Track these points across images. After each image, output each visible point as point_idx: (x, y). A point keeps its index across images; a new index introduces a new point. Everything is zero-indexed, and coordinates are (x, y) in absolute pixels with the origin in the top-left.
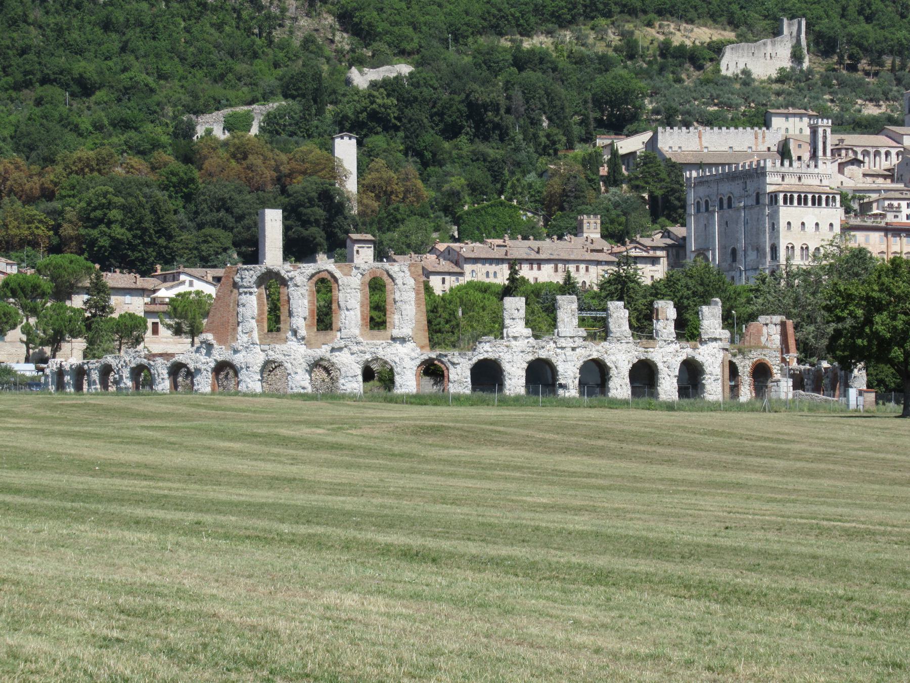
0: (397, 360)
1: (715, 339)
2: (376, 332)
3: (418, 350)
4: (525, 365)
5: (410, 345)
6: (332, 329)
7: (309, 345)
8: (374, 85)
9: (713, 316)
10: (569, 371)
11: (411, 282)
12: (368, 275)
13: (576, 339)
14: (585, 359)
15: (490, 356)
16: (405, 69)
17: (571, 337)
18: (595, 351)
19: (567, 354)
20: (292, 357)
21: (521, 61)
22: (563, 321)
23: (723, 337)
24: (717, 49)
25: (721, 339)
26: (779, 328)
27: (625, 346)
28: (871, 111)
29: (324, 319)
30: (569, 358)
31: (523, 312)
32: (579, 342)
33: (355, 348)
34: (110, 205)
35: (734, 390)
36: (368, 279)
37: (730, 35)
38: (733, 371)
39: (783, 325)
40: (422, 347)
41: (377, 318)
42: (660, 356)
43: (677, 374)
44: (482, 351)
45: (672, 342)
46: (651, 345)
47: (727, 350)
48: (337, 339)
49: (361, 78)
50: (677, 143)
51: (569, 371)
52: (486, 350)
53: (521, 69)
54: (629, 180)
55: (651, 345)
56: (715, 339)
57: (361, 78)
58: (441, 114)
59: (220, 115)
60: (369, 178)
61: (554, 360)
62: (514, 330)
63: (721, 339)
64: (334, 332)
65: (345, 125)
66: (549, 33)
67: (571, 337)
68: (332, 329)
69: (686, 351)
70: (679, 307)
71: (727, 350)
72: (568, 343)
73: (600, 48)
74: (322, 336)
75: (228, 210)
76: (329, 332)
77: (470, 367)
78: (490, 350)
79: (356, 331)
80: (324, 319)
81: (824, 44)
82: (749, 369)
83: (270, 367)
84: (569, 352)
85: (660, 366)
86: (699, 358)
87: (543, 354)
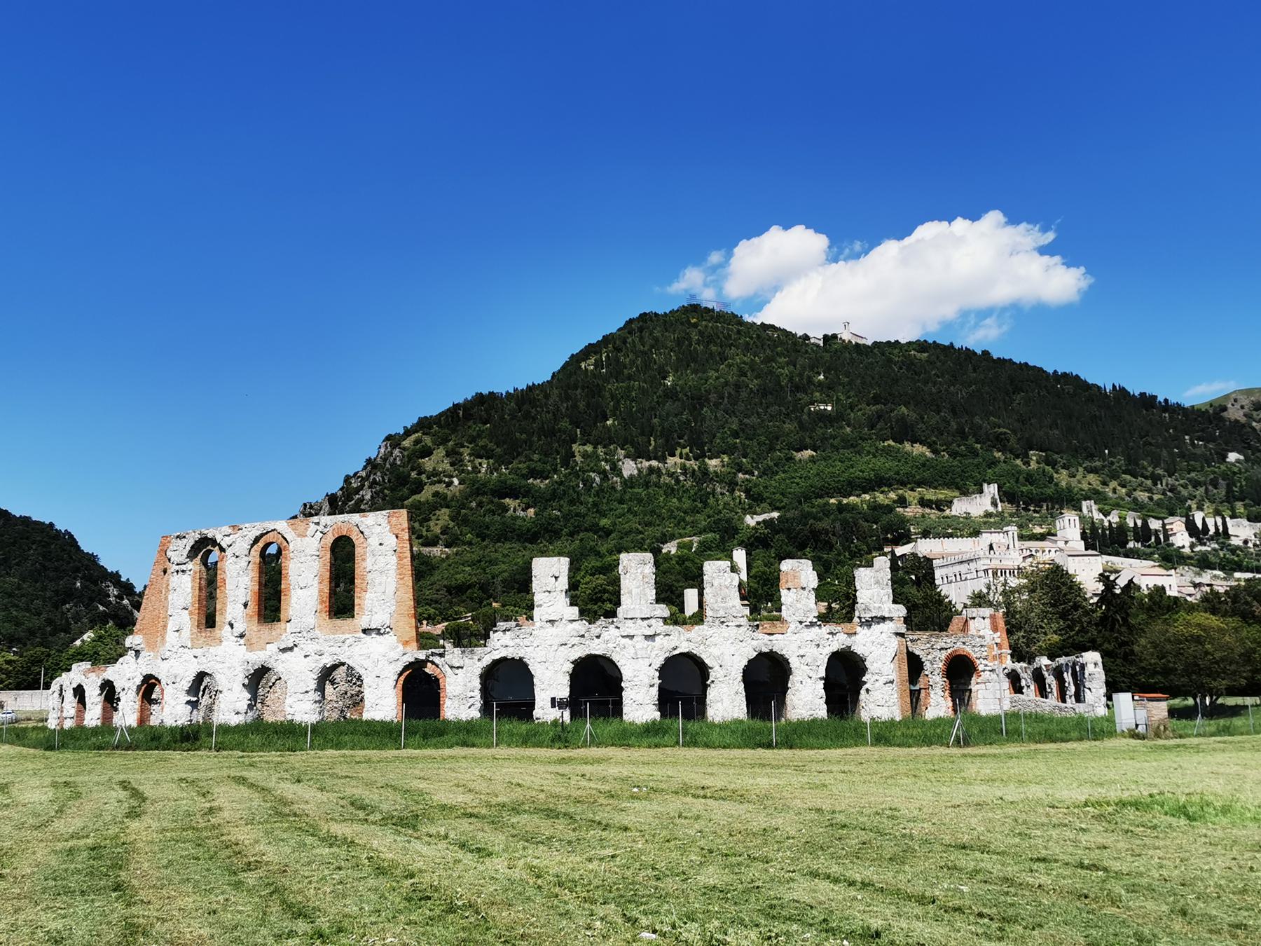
0: (367, 663)
1: (883, 619)
2: (339, 622)
3: (401, 647)
4: (569, 667)
5: (390, 639)
6: (279, 620)
7: (250, 646)
8: (758, 523)
9: (877, 582)
10: (551, 684)
11: (391, 541)
12: (330, 534)
13: (653, 621)
14: (667, 655)
15: (509, 653)
16: (775, 515)
17: (643, 619)
18: (682, 640)
19: (639, 646)
20: (227, 665)
21: (841, 508)
22: (630, 592)
23: (894, 615)
24: (949, 503)
25: (891, 619)
26: (988, 621)
27: (733, 631)
28: (1038, 530)
29: (269, 604)
30: (640, 654)
31: (564, 583)
32: (658, 626)
33: (310, 647)
34: (605, 591)
35: (915, 698)
36: (330, 539)
37: (957, 493)
38: (915, 666)
39: (993, 617)
40: (406, 643)
41: (341, 603)
42: (794, 647)
43: (823, 675)
44: (498, 645)
45: (812, 624)
46: (779, 630)
47: (902, 635)
48: (285, 632)
49: (751, 521)
50: (925, 547)
51: (551, 684)
52: (502, 644)
53: (841, 513)
54: (903, 568)
55: (779, 630)
56: (883, 619)
57: (751, 521)
58: (795, 537)
59: (675, 543)
60: (753, 571)
61: (615, 658)
62: (550, 610)
63: (891, 619)
64: (282, 625)
65: (741, 544)
66: (858, 496)
67: (643, 619)
68: (279, 620)
69: (833, 639)
70: (823, 571)
71: (902, 635)
72: (641, 629)
73: (887, 502)
74: (266, 631)
75: (672, 592)
76: (277, 625)
77: (479, 671)
78: (511, 643)
79: (311, 620)
80: (269, 604)
81: (1007, 495)
82: (941, 665)
83: (199, 683)
84: (640, 642)
85: (794, 663)
86: (859, 649)
87: (597, 648)
